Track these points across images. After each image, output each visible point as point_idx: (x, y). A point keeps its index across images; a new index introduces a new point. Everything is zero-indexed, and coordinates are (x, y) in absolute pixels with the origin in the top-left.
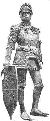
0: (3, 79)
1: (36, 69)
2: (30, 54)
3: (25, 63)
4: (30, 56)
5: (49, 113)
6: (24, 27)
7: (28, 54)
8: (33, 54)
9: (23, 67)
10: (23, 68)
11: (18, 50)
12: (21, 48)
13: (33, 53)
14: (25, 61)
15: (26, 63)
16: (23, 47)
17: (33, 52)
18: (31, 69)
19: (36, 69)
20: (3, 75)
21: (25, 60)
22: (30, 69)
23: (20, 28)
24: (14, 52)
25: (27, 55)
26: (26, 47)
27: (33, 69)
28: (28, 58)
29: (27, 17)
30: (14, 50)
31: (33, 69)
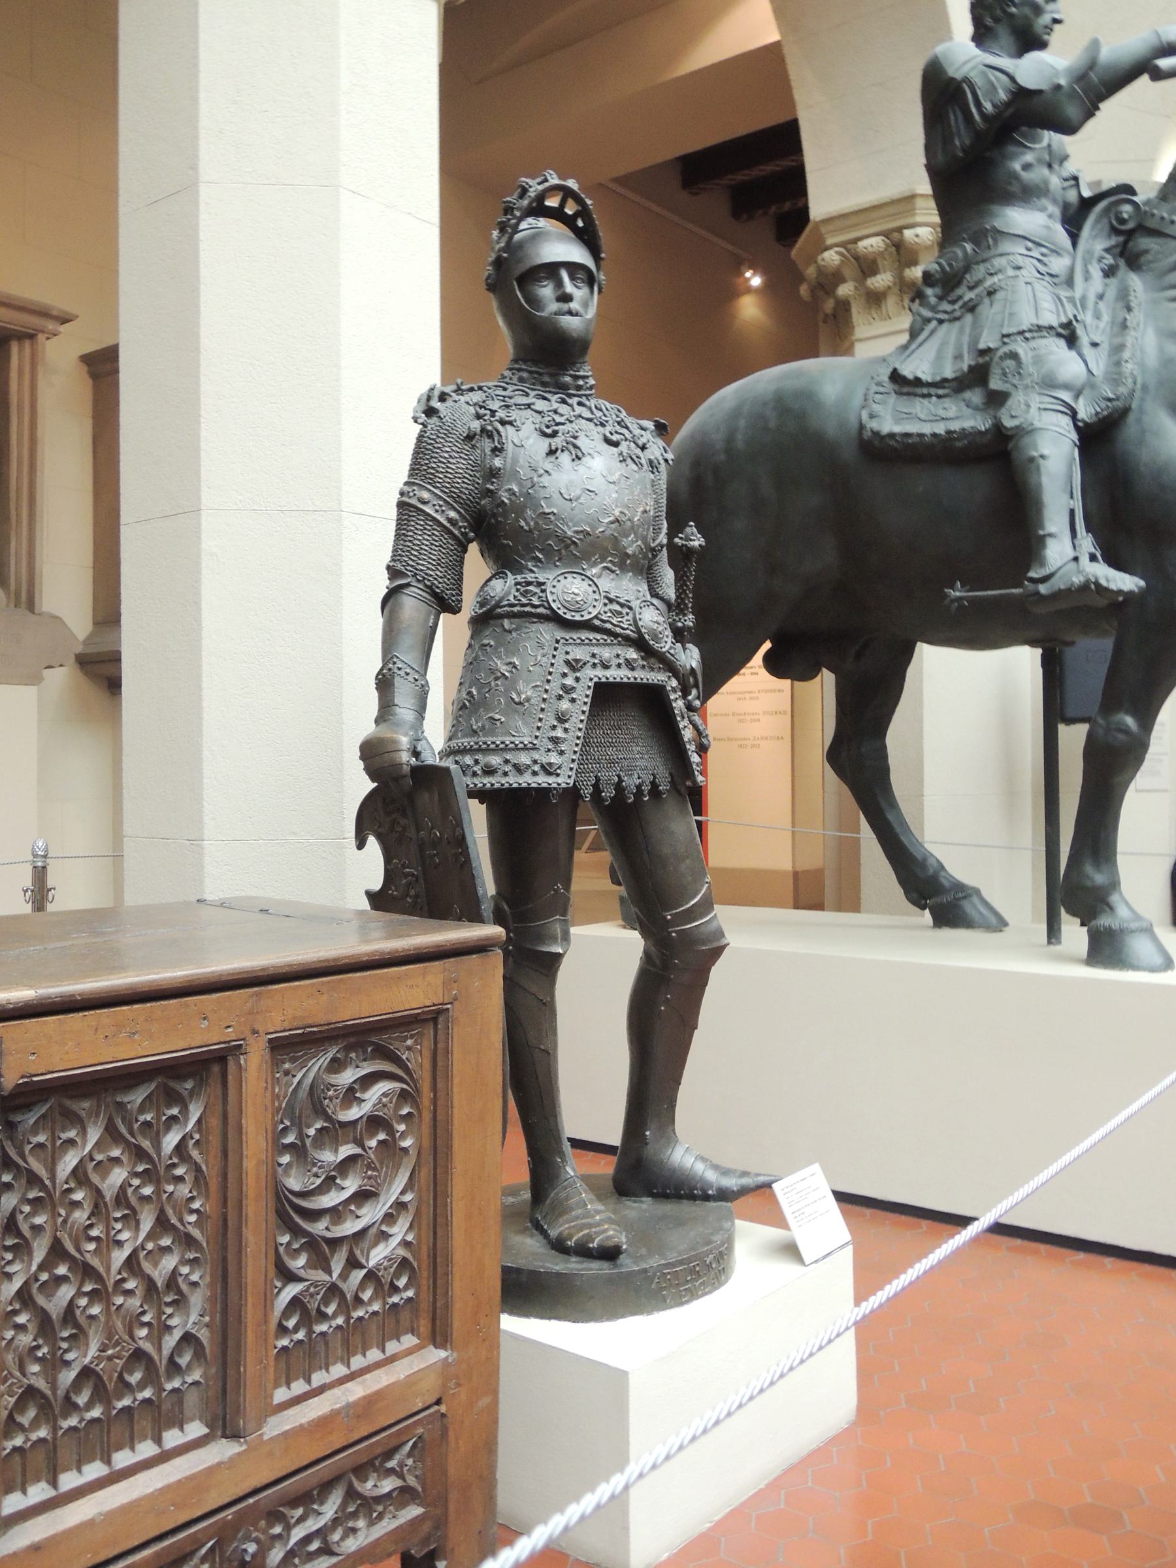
0: (377, 884)
1: (654, 785)
2: (606, 653)
3: (559, 733)
4: (600, 673)
5: (388, 1355)
6: (540, 405)
7: (578, 653)
8: (632, 654)
9: (548, 769)
10: (543, 780)
11: (487, 618)
12: (525, 594)
13: (628, 641)
14: (562, 719)
15: (571, 745)
16: (540, 584)
17: (625, 624)
18: (619, 787)
19: (654, 785)
20: (372, 841)
21: (565, 705)
22: (608, 793)
23: (501, 414)
24: (451, 634)
25: (574, 666)
26: (569, 589)
27: (631, 782)
28: (584, 693)
29: (570, 313)
30: (455, 610)
31: (631, 782)
